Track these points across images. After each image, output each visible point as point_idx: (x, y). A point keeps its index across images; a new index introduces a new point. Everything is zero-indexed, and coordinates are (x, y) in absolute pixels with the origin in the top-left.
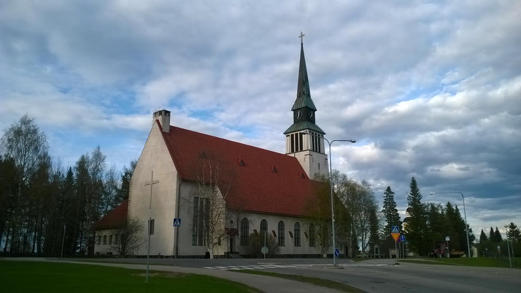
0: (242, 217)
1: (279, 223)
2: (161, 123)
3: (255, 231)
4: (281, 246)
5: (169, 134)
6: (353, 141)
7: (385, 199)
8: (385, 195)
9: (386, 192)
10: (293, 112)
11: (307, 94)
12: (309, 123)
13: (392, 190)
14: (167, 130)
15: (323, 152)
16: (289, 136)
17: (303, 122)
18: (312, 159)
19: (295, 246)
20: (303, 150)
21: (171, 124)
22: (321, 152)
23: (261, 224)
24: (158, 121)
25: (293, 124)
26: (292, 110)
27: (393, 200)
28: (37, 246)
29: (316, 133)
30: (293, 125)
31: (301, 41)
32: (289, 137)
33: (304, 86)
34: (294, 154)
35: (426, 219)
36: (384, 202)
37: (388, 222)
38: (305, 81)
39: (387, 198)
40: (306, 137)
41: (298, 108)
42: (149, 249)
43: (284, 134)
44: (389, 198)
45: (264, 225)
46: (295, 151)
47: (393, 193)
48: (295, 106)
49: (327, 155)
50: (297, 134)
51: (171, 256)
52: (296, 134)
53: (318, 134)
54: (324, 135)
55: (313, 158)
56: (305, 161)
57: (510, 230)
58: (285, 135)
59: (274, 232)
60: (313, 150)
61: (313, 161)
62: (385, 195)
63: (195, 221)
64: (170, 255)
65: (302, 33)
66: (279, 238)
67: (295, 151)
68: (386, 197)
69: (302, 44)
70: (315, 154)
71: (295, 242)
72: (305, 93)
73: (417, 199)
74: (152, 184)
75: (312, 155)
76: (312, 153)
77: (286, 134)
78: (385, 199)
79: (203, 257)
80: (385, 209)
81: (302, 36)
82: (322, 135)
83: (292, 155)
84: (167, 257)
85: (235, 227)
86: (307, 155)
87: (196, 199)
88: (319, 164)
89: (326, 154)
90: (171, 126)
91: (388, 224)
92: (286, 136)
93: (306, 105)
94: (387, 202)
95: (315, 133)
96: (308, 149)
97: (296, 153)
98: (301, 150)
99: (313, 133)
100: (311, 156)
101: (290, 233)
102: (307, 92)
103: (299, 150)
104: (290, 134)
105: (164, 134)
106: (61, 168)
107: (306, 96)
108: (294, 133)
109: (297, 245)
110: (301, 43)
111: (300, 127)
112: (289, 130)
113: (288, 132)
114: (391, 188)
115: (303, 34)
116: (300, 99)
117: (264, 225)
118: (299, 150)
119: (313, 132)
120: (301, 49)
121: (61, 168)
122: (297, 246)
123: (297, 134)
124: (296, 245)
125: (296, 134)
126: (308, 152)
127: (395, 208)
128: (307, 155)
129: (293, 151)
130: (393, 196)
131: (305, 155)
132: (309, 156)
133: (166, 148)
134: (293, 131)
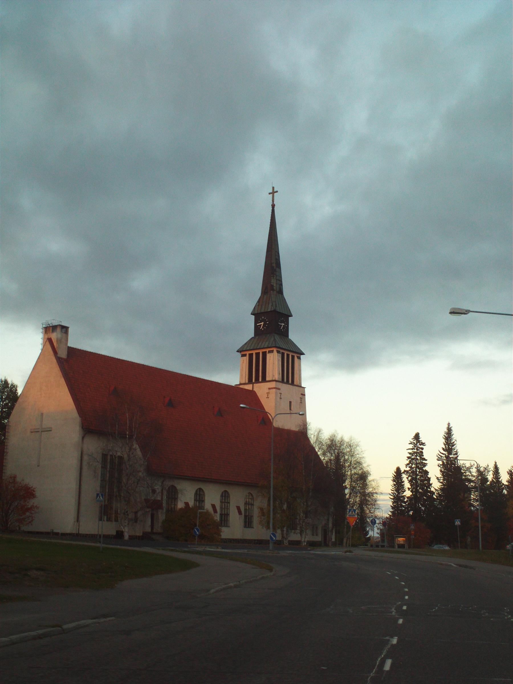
0: (168, 483)
1: (222, 493)
2: (55, 344)
3: (187, 504)
4: (224, 526)
5: (67, 360)
6: (302, 414)
7: (410, 453)
8: (411, 446)
9: (412, 441)
10: (253, 317)
11: (278, 290)
12: (277, 337)
13: (422, 439)
14: (63, 354)
15: (298, 384)
17: (268, 335)
18: (279, 395)
19: (245, 526)
20: (267, 379)
21: (70, 344)
22: (295, 383)
23: (196, 494)
24: (50, 340)
27: (423, 456)
28: (163, 502)
29: (289, 353)
32: (245, 358)
33: (273, 277)
34: (251, 385)
35: (503, 489)
36: (408, 458)
37: (411, 491)
38: (275, 268)
39: (414, 450)
40: (272, 358)
41: (263, 311)
43: (238, 351)
44: (416, 451)
45: (200, 496)
46: (254, 381)
49: (305, 388)
50: (258, 354)
51: (70, 534)
52: (256, 353)
53: (291, 354)
54: (302, 356)
55: (281, 394)
56: (268, 398)
58: (239, 353)
59: (213, 506)
60: (282, 381)
61: (281, 398)
62: (411, 446)
63: (102, 487)
64: (68, 531)
65: (273, 188)
66: (221, 515)
67: (254, 381)
68: (412, 449)
69: (273, 206)
70: (284, 387)
71: (245, 522)
72: (275, 288)
73: (452, 458)
74: (42, 431)
75: (279, 389)
76: (280, 385)
77: (240, 352)
78: (410, 453)
79: (113, 537)
80: (408, 469)
81: (273, 193)
82: (298, 355)
83: (249, 387)
84: (64, 535)
85: (159, 498)
86: (272, 388)
87: (104, 456)
88: (290, 402)
89: (302, 386)
90: (68, 347)
91: (411, 493)
92: (241, 356)
93: (274, 308)
94: (413, 457)
95: (286, 353)
96: (274, 379)
97: (254, 385)
98: (264, 380)
99: (283, 354)
100: (278, 391)
101: (238, 508)
102: (278, 285)
103: (260, 380)
104: (248, 353)
105: (60, 360)
107: (275, 292)
108: (254, 352)
109: (247, 526)
110: (271, 203)
111: (264, 343)
112: (246, 346)
113: (245, 349)
114: (420, 435)
115: (275, 190)
117: (200, 496)
118: (260, 380)
119: (283, 351)
120: (271, 214)
122: (248, 527)
123: (258, 354)
124: (246, 525)
125: (256, 353)
126: (273, 384)
127: (424, 469)
128: (272, 388)
129: (250, 381)
130: (422, 449)
131: (269, 389)
132: (274, 390)
133: (62, 381)
134: (252, 348)
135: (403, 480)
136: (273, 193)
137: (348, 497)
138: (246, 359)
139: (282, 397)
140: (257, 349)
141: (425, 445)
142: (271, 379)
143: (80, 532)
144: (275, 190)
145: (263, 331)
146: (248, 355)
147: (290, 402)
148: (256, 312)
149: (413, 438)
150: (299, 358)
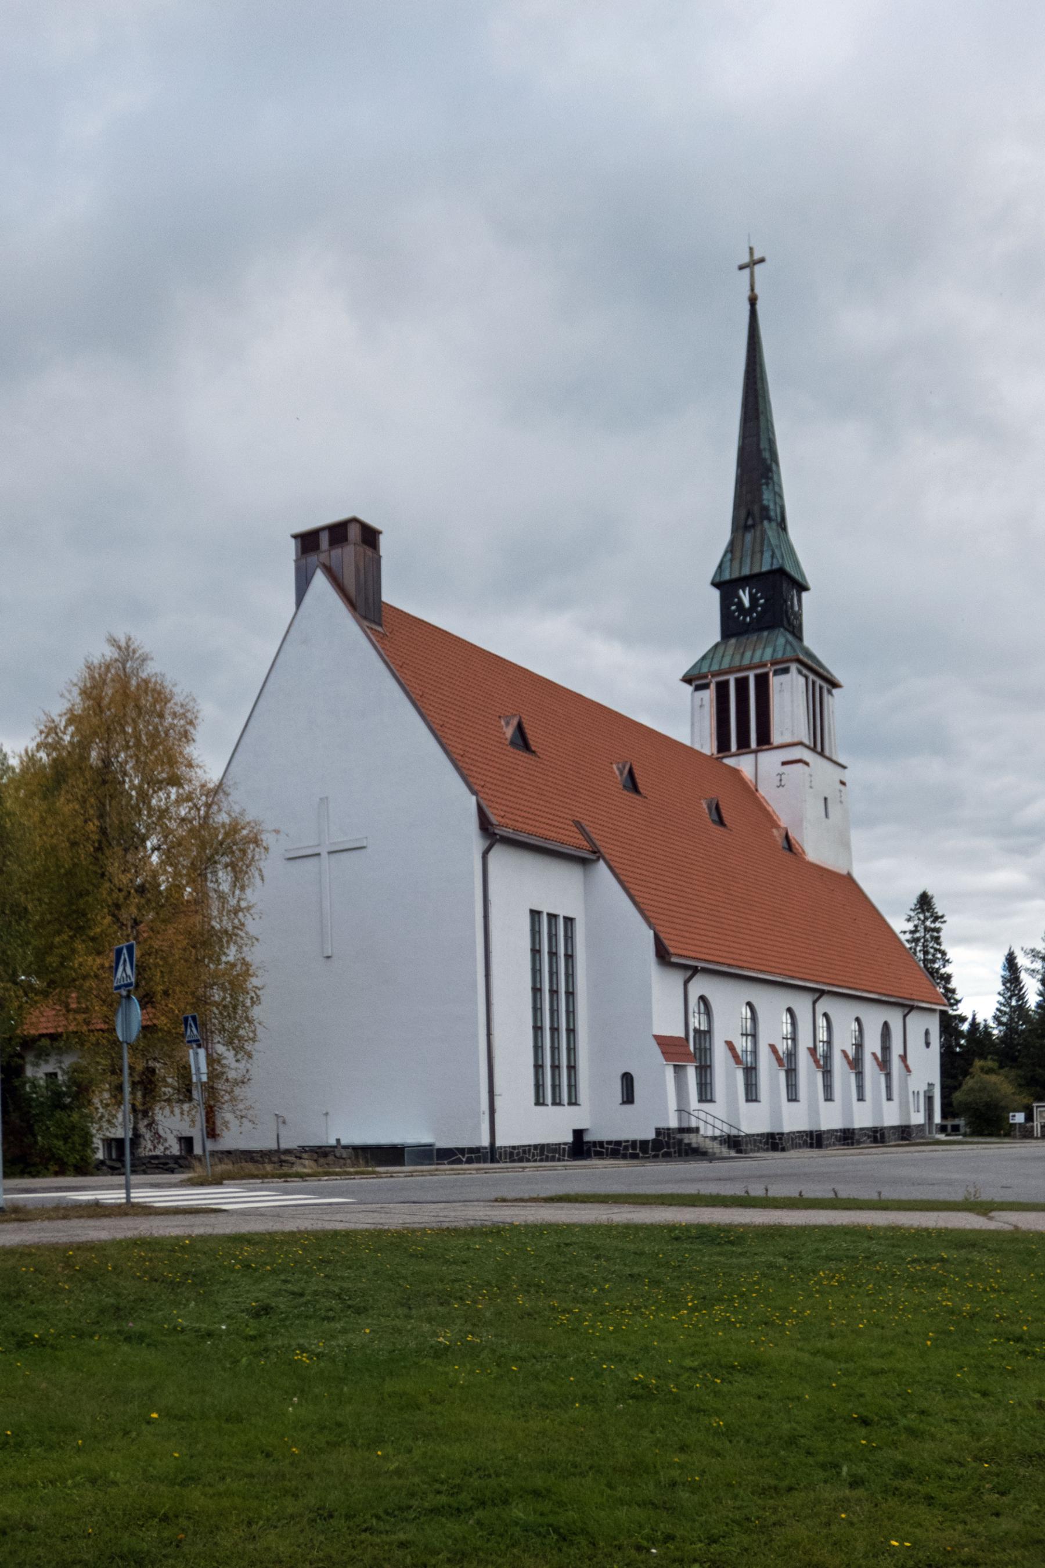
16: (706, 686)
20: (776, 738)
25: (717, 637)
26: (716, 584)
30: (721, 649)
31: (748, 288)
38: (769, 462)
41: (746, 571)
42: (516, 1200)
47: (942, 917)
48: (727, 564)
50: (742, 685)
54: (835, 691)
57: (142, 1119)
69: (753, 301)
72: (772, 514)
82: (830, 687)
106: (774, 1495)
110: (747, 293)
116: (749, 537)
118: (753, 744)
121: (774, 1495)
123: (742, 685)
125: (737, 680)
130: (938, 930)
135: (1041, 998)
136: (753, 263)
137: (997, 1041)
138: (708, 696)
139: (813, 784)
140: (740, 669)
141: (942, 920)
142: (788, 739)
143: (499, 1143)
144: (757, 256)
145: (749, 624)
146: (713, 686)
147: (826, 799)
148: (727, 576)
149: (913, 907)
150: (830, 692)
